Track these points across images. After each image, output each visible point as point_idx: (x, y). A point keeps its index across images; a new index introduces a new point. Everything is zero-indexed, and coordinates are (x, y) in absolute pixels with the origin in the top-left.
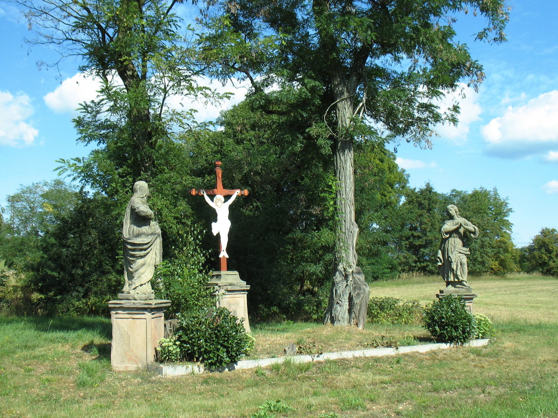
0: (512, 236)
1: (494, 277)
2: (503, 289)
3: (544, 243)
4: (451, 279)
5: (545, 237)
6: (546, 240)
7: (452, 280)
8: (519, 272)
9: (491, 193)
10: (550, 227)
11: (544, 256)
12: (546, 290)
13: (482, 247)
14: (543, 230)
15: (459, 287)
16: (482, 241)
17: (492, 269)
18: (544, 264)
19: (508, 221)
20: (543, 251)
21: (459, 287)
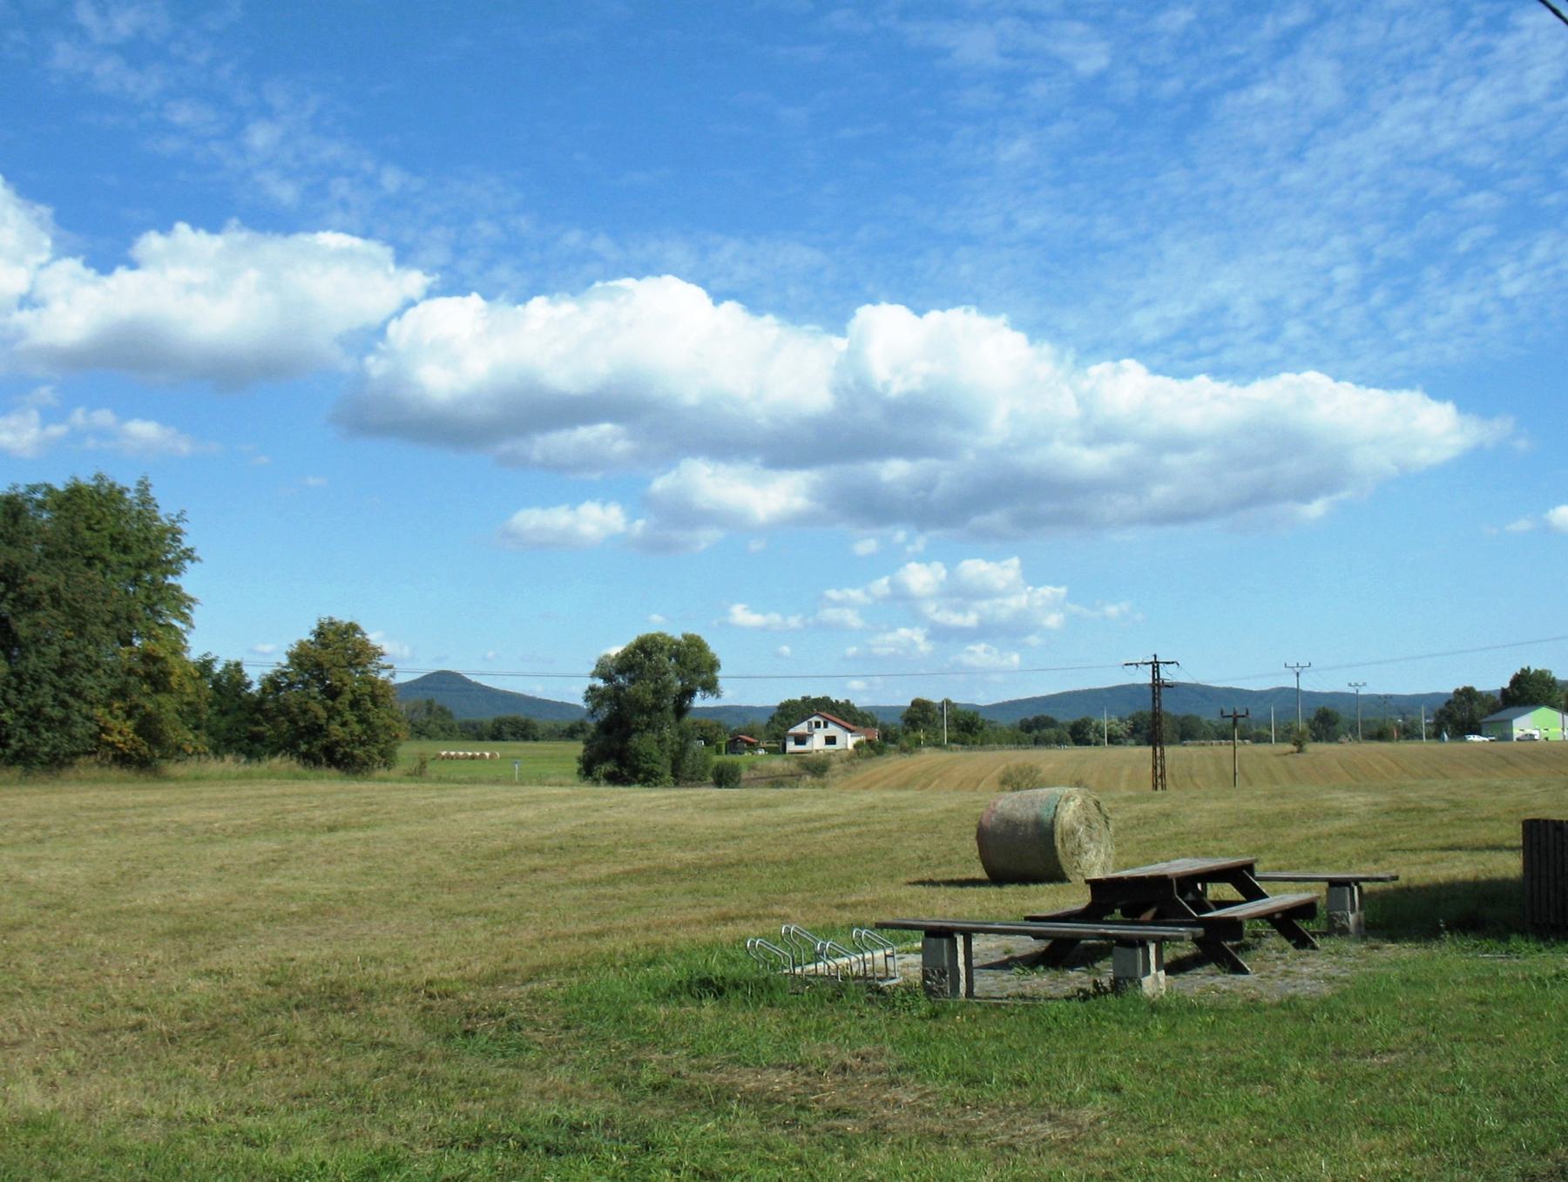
10: (343, 617)
14: (321, 626)
18: (315, 730)
19: (178, 589)
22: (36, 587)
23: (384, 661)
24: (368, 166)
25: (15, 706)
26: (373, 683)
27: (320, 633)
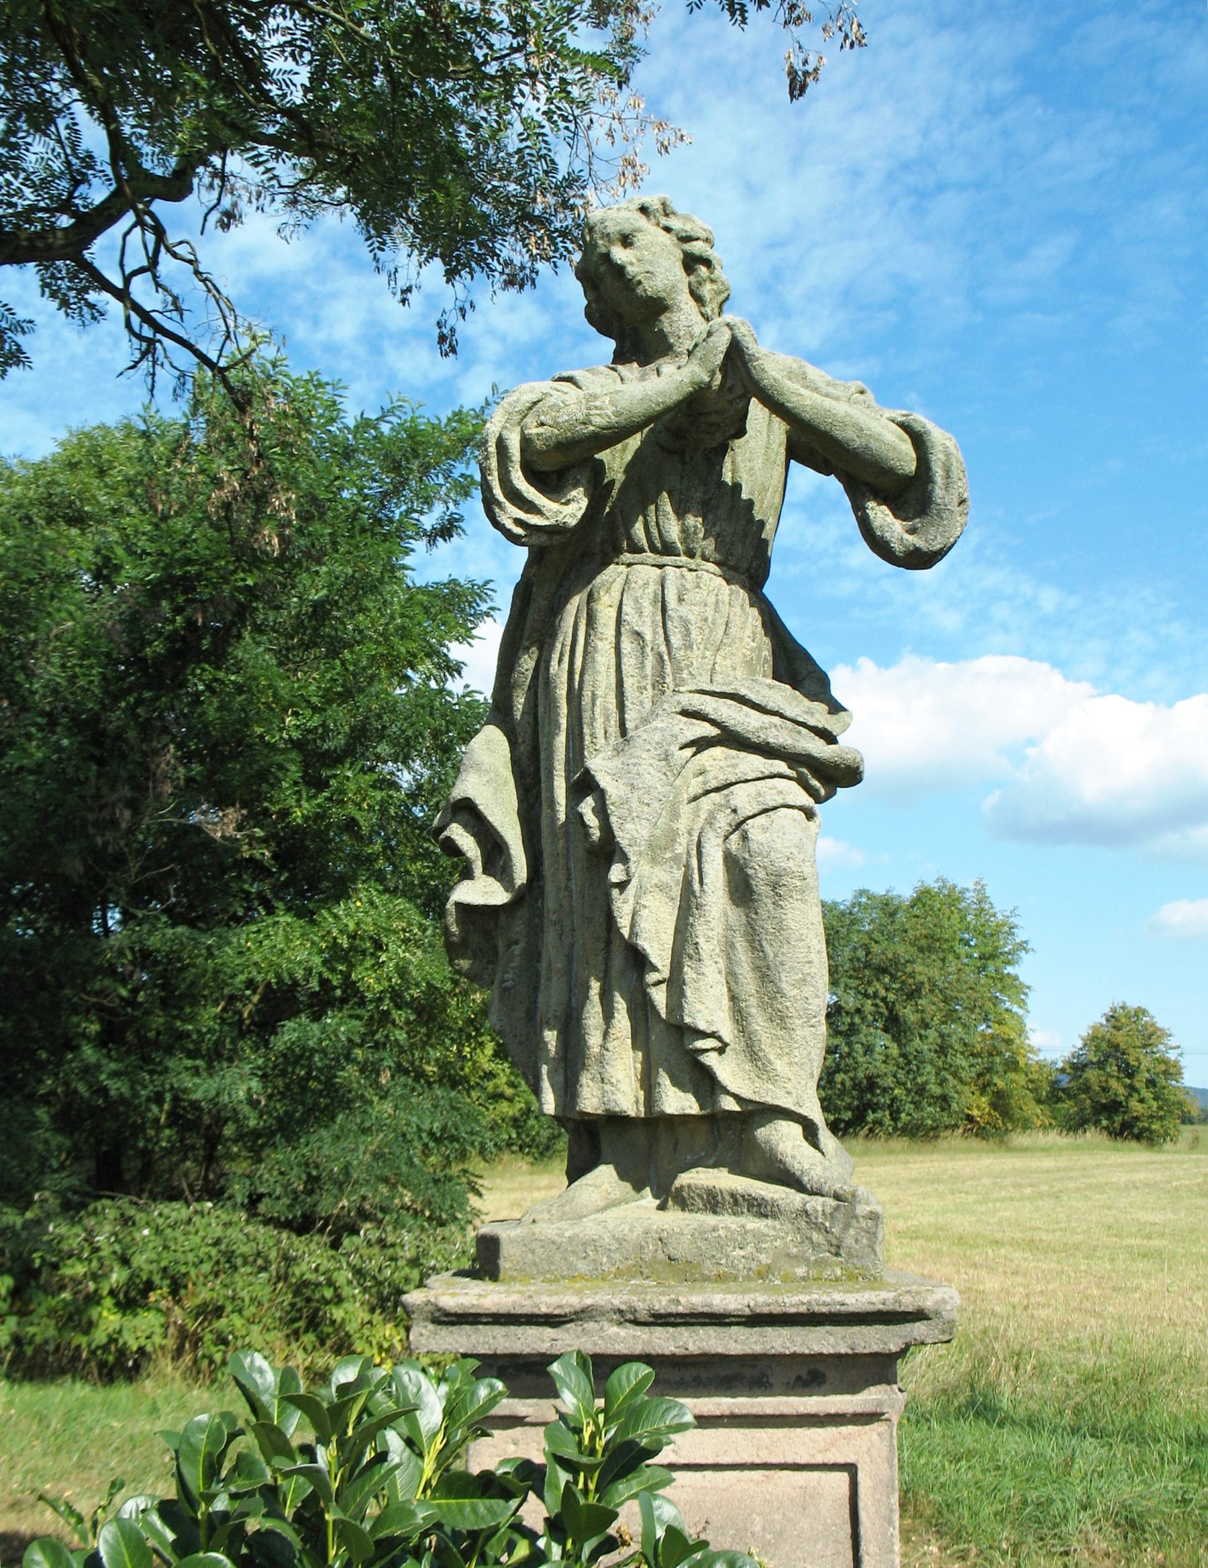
0: (1030, 1023)
1: (975, 1143)
2: (1008, 1181)
3: (1116, 1047)
4: (616, 1080)
5: (1118, 1028)
6: (1120, 1038)
7: (628, 1101)
8: (1045, 1128)
9: (968, 895)
10: (1133, 1003)
11: (1113, 1083)
12: (1147, 1185)
13: (942, 1050)
14: (1114, 1010)
15: (713, 1202)
16: (942, 1036)
17: (970, 1119)
18: (1113, 1107)
19: (1016, 978)
20: (1112, 1069)
21: (713, 1202)
22: (919, 978)
23: (1172, 1042)
24: (1027, 588)
25: (904, 1084)
26: (1165, 1062)
27: (1112, 1018)
